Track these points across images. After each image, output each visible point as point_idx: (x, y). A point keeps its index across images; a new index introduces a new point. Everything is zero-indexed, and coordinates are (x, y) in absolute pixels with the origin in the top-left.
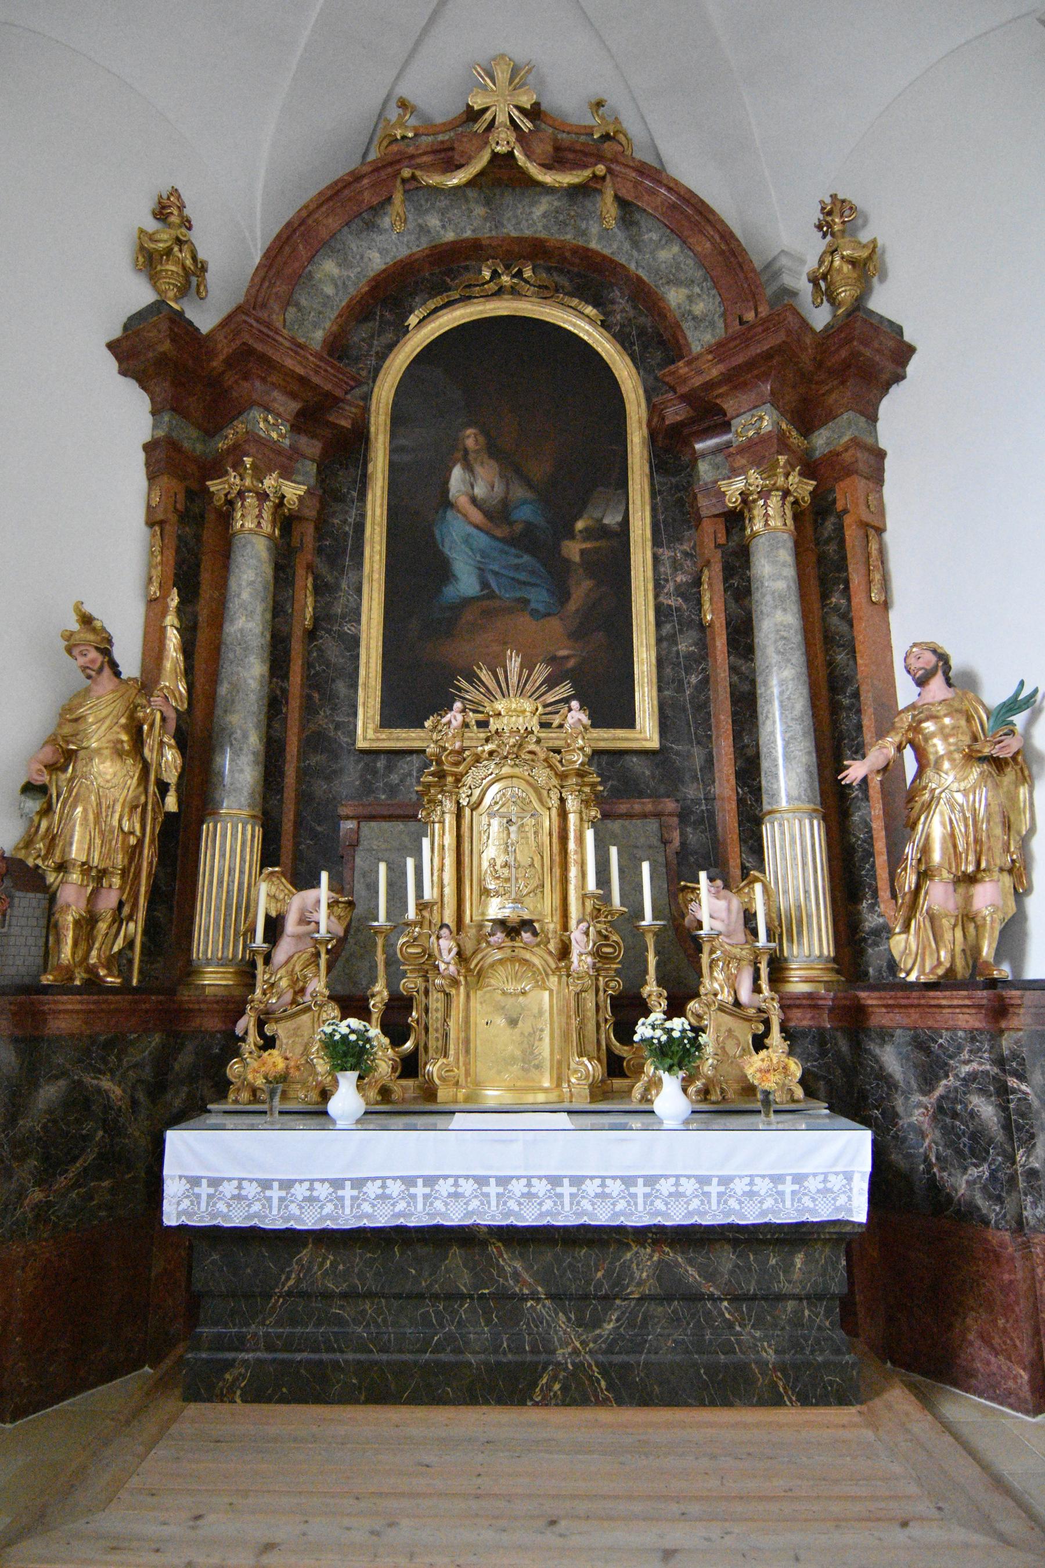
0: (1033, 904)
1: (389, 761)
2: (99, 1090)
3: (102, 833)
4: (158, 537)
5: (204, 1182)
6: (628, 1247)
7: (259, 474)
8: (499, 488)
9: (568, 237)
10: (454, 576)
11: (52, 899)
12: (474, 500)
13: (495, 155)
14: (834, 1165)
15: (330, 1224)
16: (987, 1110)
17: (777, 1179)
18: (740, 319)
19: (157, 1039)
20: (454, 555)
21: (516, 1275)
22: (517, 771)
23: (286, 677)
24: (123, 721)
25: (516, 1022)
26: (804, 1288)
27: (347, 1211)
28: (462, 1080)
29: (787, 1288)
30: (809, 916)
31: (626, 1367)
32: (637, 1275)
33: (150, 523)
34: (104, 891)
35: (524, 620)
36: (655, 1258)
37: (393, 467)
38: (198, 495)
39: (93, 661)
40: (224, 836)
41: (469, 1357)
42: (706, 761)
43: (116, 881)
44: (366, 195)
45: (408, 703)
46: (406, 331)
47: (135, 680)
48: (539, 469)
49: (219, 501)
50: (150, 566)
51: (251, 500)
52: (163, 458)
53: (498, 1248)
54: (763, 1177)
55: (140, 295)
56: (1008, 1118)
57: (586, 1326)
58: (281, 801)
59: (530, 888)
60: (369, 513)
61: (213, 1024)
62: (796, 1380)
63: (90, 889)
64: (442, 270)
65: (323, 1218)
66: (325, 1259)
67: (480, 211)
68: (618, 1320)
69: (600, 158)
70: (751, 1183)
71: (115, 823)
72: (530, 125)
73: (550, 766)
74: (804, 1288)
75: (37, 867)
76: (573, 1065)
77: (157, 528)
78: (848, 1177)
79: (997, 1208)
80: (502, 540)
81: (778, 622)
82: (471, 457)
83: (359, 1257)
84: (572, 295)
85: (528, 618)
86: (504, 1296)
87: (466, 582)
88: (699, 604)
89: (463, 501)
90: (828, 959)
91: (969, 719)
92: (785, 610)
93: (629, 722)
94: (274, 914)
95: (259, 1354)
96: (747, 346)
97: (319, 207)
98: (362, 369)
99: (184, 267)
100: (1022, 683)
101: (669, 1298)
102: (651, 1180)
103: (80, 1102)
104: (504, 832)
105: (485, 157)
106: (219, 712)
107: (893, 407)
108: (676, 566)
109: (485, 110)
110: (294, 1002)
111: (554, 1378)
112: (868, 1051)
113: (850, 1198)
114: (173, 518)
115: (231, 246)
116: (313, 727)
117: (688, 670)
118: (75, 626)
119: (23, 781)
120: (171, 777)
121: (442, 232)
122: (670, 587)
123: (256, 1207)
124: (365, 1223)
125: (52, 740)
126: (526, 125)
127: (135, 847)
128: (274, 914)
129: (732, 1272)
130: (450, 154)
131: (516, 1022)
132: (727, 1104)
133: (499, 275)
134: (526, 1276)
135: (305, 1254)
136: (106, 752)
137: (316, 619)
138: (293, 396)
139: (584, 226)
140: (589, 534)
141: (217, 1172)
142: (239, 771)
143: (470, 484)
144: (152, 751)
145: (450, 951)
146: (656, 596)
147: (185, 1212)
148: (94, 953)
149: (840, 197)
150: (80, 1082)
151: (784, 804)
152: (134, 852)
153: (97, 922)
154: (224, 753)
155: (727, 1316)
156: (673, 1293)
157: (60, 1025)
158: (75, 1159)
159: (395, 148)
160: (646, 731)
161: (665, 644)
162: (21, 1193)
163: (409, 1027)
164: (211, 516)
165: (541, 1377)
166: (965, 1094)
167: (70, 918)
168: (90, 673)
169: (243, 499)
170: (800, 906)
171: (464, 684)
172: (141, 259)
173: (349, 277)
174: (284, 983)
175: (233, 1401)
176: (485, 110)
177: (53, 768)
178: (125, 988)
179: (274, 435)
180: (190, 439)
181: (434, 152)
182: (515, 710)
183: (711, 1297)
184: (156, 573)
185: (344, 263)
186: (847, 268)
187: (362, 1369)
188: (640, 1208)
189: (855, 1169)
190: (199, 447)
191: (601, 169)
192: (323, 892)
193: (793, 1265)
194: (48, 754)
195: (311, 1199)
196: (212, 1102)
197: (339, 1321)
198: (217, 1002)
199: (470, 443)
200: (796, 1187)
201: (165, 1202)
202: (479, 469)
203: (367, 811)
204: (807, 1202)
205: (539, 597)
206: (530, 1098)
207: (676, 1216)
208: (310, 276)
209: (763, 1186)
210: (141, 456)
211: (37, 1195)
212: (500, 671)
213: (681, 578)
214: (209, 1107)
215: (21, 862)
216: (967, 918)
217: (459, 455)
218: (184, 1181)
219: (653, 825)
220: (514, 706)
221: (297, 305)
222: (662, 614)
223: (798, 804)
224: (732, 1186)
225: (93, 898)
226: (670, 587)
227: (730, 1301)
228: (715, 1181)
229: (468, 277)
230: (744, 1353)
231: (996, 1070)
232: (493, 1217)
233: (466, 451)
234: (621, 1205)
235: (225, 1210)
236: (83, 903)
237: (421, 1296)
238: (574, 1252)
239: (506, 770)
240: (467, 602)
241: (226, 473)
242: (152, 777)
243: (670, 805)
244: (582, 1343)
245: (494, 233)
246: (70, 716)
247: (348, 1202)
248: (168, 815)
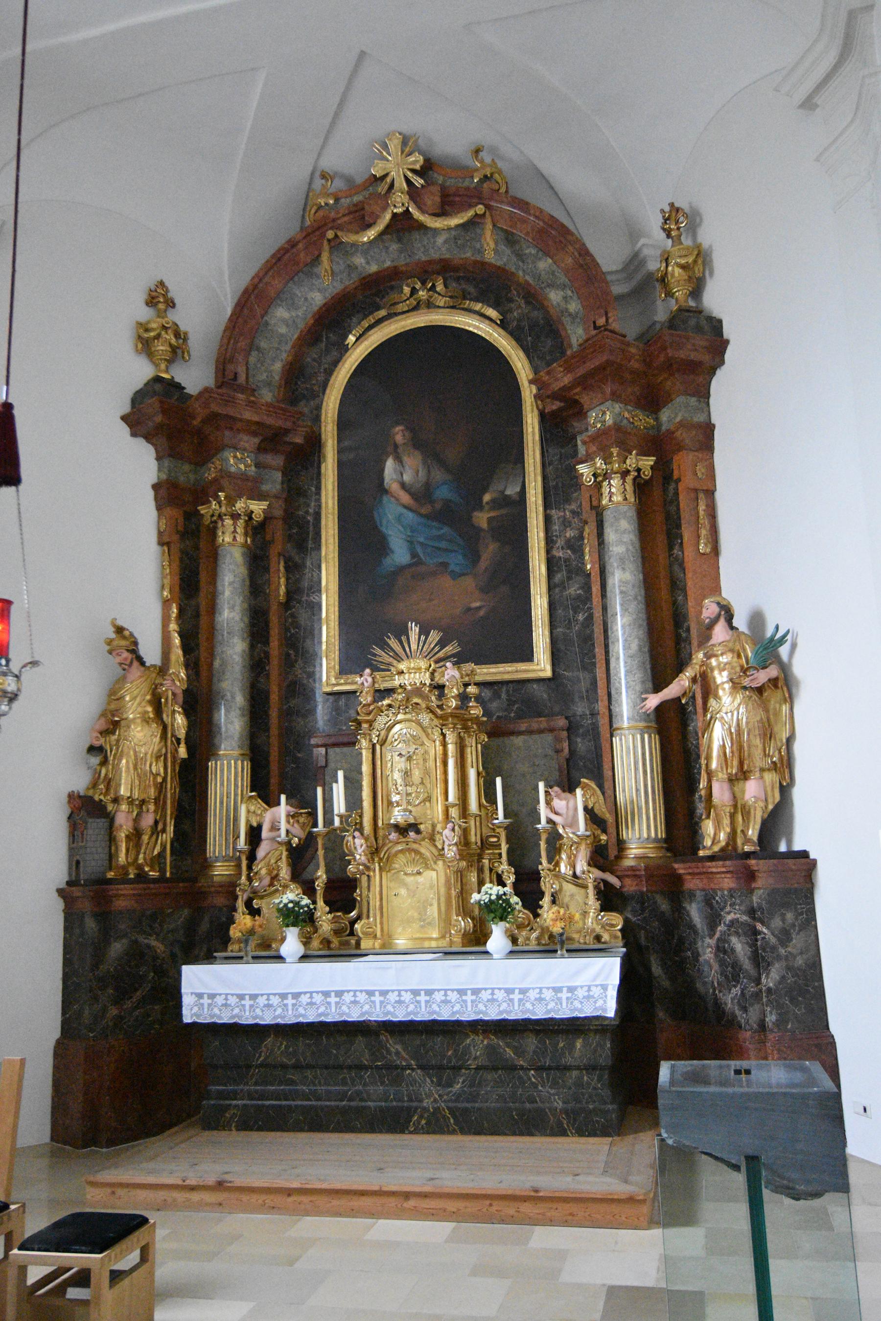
0: (798, 794)
1: (348, 700)
2: (149, 946)
3: (138, 775)
4: (167, 554)
5: (206, 996)
6: (467, 1036)
7: (231, 501)
8: (422, 473)
9: (469, 255)
10: (390, 549)
11: (112, 820)
12: (403, 485)
13: (395, 215)
14: (594, 980)
15: (280, 1021)
16: (739, 946)
17: (557, 990)
18: (594, 323)
19: (186, 912)
20: (390, 533)
21: (397, 1053)
22: (408, 716)
23: (267, 642)
24: (148, 697)
25: (411, 894)
26: (582, 1062)
27: (290, 1012)
28: (379, 934)
29: (568, 1060)
30: (640, 809)
31: (466, 1110)
32: (473, 1053)
33: (161, 543)
34: (144, 815)
35: (446, 582)
36: (485, 1042)
38: (191, 516)
39: (126, 659)
40: (222, 771)
41: (370, 1103)
42: (592, 684)
43: (152, 807)
44: (302, 255)
45: (354, 660)
46: (346, 349)
47: (154, 666)
48: (453, 455)
49: (207, 521)
50: (163, 577)
51: (228, 522)
52: (167, 494)
53: (386, 1036)
54: (548, 988)
55: (141, 371)
56: (756, 951)
57: (444, 1087)
58: (268, 737)
59: (420, 799)
60: (323, 505)
61: (220, 901)
62: (575, 1120)
63: (135, 813)
64: (367, 297)
65: (275, 1018)
66: (281, 1045)
67: (394, 247)
68: (463, 1083)
69: (480, 200)
70: (541, 992)
71: (148, 768)
72: (422, 182)
73: (432, 712)
74: (582, 1062)
75: (101, 800)
76: (453, 922)
77: (166, 548)
78: (605, 988)
79: (744, 1015)
80: (427, 516)
82: (400, 450)
83: (301, 1043)
84: (477, 300)
85: (449, 577)
86: (390, 1067)
88: (582, 555)
89: (395, 487)
90: (656, 840)
91: (739, 656)
92: (624, 569)
93: (527, 655)
94: (255, 824)
95: (244, 1102)
96: (584, 363)
97: (266, 273)
98: (314, 384)
99: (171, 345)
100: (777, 628)
101: (495, 1069)
102: (476, 992)
103: (137, 953)
104: (410, 763)
105: (388, 217)
106: (215, 680)
107: (721, 385)
108: (566, 524)
109: (386, 175)
110: (271, 884)
111: (421, 1117)
112: (684, 908)
113: (605, 1002)
114: (176, 538)
115: (202, 316)
116: (291, 677)
117: (576, 611)
118: (113, 636)
119: (87, 746)
120: (182, 733)
121: (367, 267)
122: (560, 543)
123: (236, 1011)
124: (301, 1020)
125: (103, 714)
126: (419, 182)
127: (161, 784)
128: (255, 824)
129: (534, 1052)
130: (362, 212)
133: (418, 291)
134: (403, 1053)
135: (270, 1040)
136: (139, 721)
137: (288, 593)
138: (254, 434)
139: (478, 246)
140: (496, 504)
141: (212, 991)
142: (231, 722)
143: (399, 472)
144: (168, 716)
145: (361, 846)
146: (548, 552)
147: (195, 1014)
148: (141, 856)
149: (676, 205)
150: (136, 941)
151: (626, 724)
152: (161, 788)
153: (142, 834)
154: (219, 710)
155: (533, 1080)
156: (495, 1064)
157: (121, 904)
158: (136, 990)
159: (321, 213)
160: (542, 664)
161: (557, 590)
162: (105, 1010)
163: (355, 900)
164: (203, 530)
165: (413, 1115)
166: (729, 935)
167: (123, 835)
168: (125, 667)
169: (223, 520)
170: (633, 801)
171: (378, 651)
172: (140, 346)
173: (297, 316)
174: (264, 872)
175: (231, 1130)
176: (386, 175)
177: (106, 733)
178: (162, 879)
179: (242, 466)
180: (186, 474)
181: (350, 213)
182: (414, 668)
183: (522, 1068)
184: (167, 581)
185: (292, 306)
186: (678, 271)
187: (306, 1110)
188: (469, 1009)
189: (609, 982)
190: (192, 477)
191: (480, 209)
192: (283, 808)
193: (574, 1046)
194: (102, 725)
195: (268, 1006)
196: (216, 951)
197: (292, 1082)
198: (221, 886)
199: (399, 438)
200: (570, 995)
201: (184, 1008)
202: (405, 459)
203: (332, 740)
204: (577, 1004)
205: (456, 561)
206: (426, 944)
207: (493, 1014)
208: (267, 324)
209: (548, 995)
210: (151, 494)
211: (113, 1011)
212: (403, 638)
213: (569, 533)
214: (215, 954)
215: (91, 798)
216: (739, 808)
217: (390, 449)
218: (194, 996)
219: (549, 738)
220: (412, 665)
221: (258, 349)
222: (552, 564)
223: (633, 723)
224: (528, 994)
225: (137, 820)
226: (560, 543)
227: (535, 1070)
228: (517, 991)
229: (394, 296)
230: (543, 1102)
231: (745, 918)
232: (378, 1016)
233: (396, 446)
234: (457, 1007)
235: (218, 1013)
236: (130, 824)
237: (341, 1067)
238: (432, 1039)
239: (400, 717)
240: (401, 569)
241: (210, 502)
242: (169, 735)
244: (439, 1096)
245: (408, 260)
246: (114, 695)
247: (290, 1007)
248: (184, 760)
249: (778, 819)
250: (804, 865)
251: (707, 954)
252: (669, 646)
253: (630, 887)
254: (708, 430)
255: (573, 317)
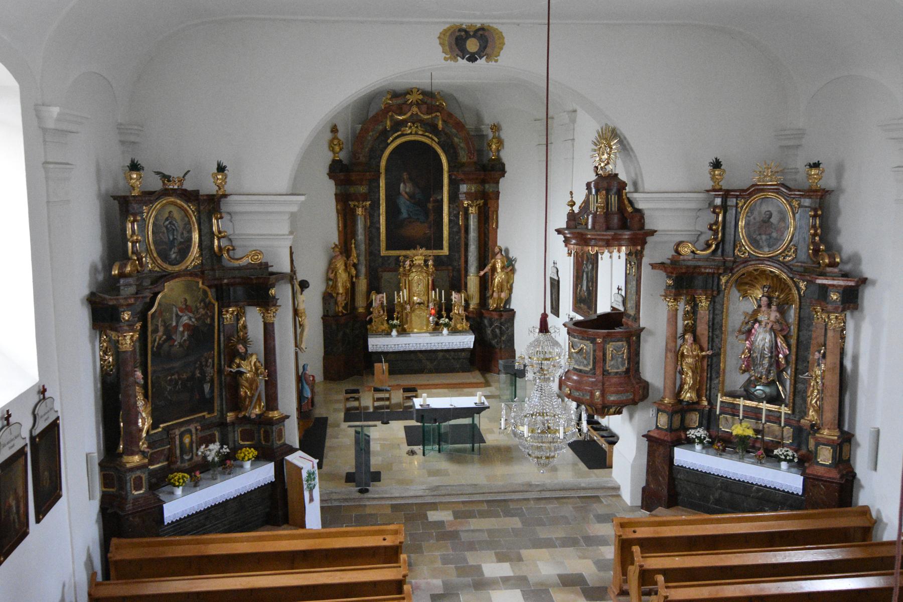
0: (513, 295)
16: (497, 331)
25: (422, 318)
37: (387, 184)
46: (389, 144)
81: (473, 235)
87: (405, 215)
93: (442, 249)
104: (417, 286)
105: (409, 114)
107: (502, 181)
108: (454, 209)
131: (422, 318)
132: (454, 331)
143: (405, 188)
160: (445, 251)
207: (445, 348)
216: (499, 298)
240: (405, 219)
243: (450, 268)
249: (508, 301)
250: (512, 313)
251: (489, 331)
252: (484, 258)
253: (471, 315)
254: (498, 193)
255: (462, 148)
